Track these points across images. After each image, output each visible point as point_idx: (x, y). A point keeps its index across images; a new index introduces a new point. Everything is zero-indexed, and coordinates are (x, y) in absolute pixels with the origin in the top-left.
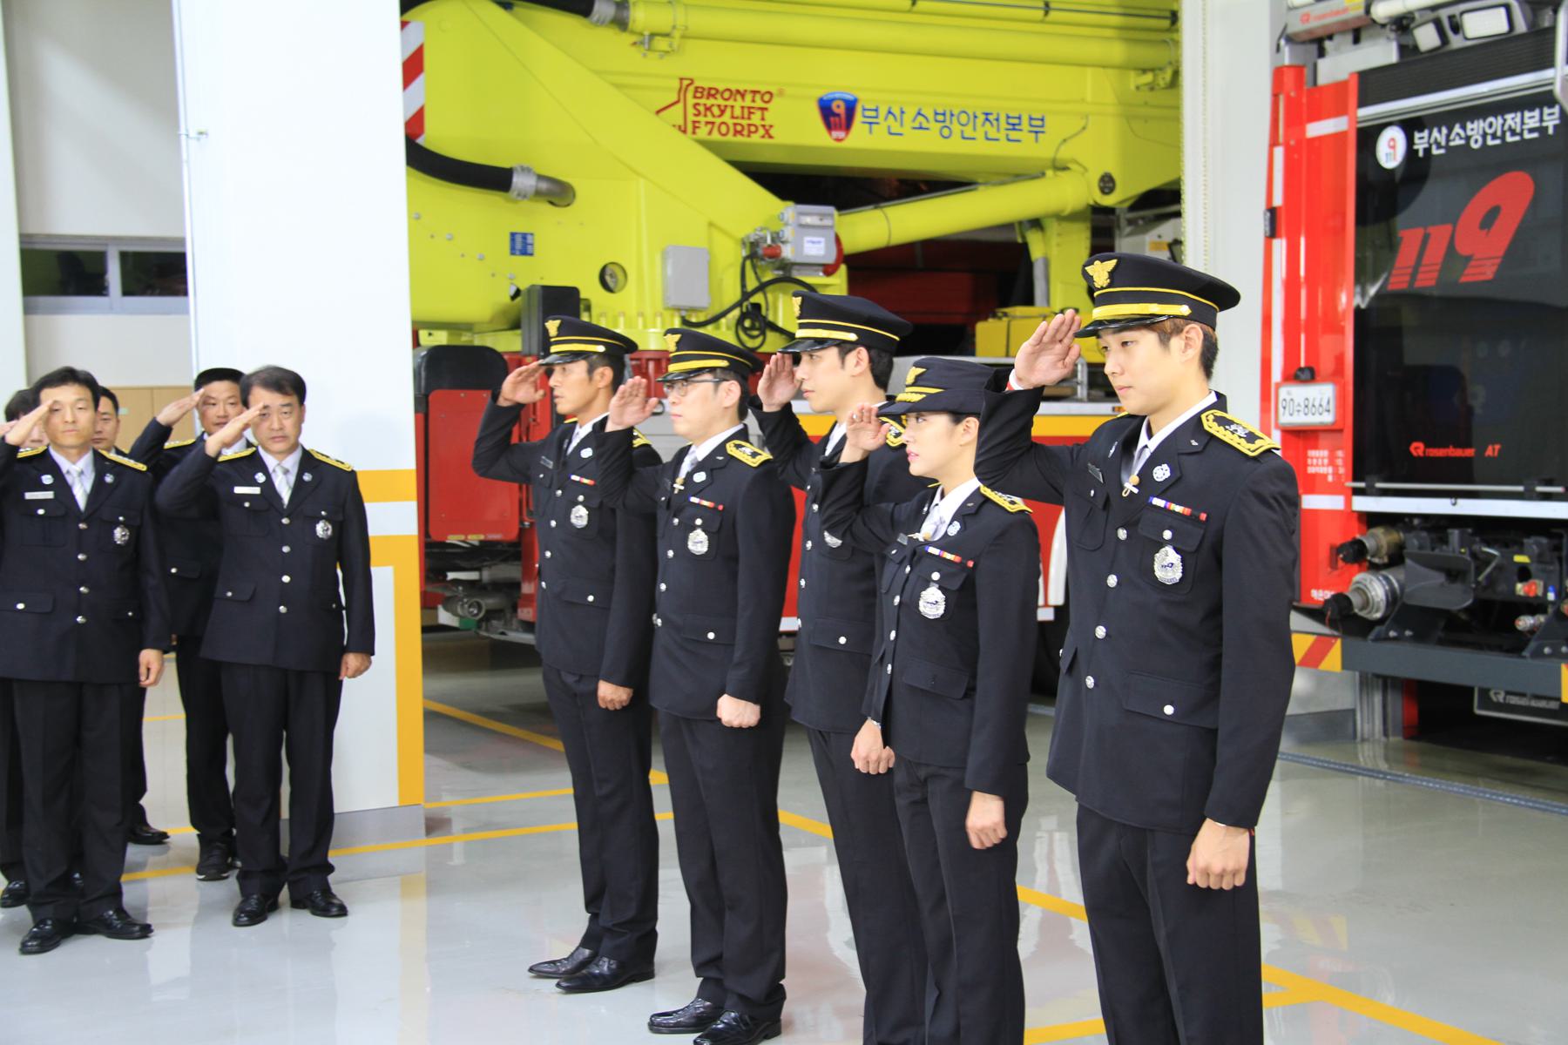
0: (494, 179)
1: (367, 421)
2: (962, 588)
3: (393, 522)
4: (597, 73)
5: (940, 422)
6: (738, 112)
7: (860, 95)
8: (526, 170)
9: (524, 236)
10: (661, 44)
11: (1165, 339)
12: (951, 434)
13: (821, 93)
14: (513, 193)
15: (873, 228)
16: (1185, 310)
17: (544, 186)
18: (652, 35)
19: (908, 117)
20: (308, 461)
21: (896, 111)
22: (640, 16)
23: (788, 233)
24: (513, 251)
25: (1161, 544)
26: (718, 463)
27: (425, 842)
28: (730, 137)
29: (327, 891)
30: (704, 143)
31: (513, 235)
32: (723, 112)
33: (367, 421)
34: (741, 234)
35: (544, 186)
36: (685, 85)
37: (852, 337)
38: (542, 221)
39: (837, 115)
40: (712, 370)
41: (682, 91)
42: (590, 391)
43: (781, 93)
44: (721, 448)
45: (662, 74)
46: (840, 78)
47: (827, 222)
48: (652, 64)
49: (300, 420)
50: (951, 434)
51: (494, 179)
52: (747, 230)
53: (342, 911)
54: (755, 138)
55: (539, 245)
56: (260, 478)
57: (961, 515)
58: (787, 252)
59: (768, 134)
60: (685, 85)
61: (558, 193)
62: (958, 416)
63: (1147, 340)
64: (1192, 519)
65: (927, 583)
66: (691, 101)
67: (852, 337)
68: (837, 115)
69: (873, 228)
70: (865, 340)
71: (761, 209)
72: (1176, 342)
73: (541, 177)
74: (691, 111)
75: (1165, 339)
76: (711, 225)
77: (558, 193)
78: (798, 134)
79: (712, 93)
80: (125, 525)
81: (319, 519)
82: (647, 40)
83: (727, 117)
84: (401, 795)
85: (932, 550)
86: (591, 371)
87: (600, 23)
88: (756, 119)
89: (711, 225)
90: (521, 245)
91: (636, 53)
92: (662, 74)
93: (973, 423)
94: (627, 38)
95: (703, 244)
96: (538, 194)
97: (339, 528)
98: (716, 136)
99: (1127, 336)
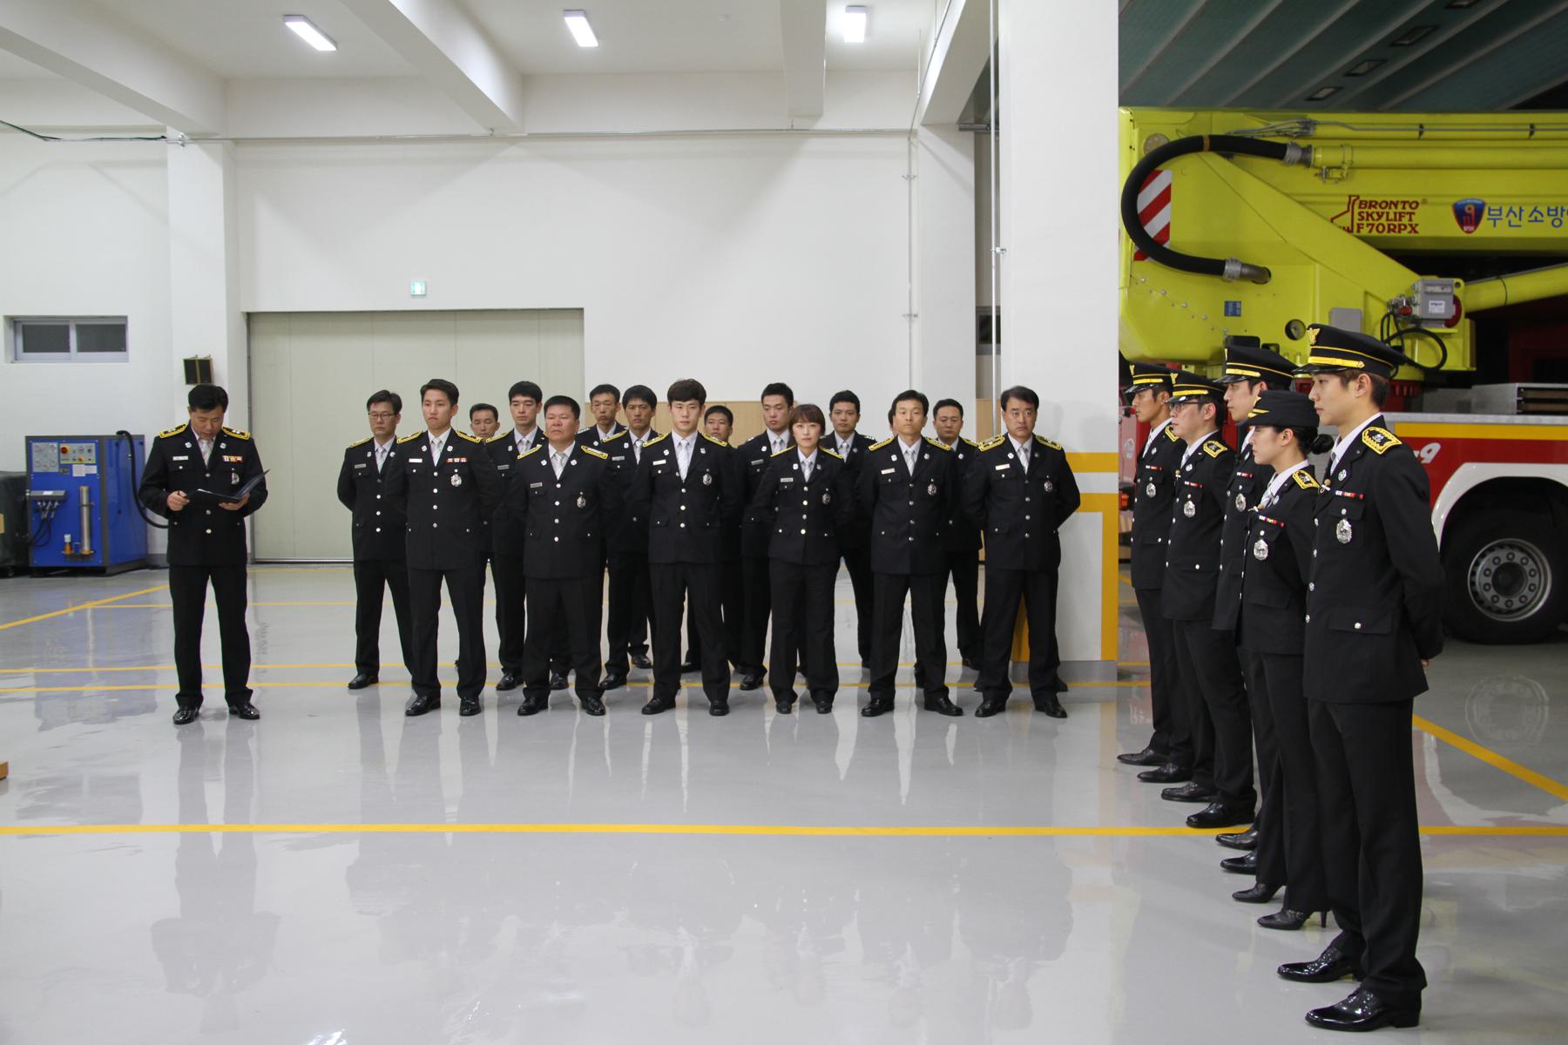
0: (1211, 267)
1: (1085, 419)
2: (1277, 540)
3: (1099, 484)
4: (1287, 195)
5: (1268, 432)
6: (1392, 216)
7: (1486, 200)
8: (1235, 261)
9: (1235, 304)
10: (1336, 174)
11: (1345, 383)
12: (1274, 440)
13: (1454, 200)
14: (1225, 276)
15: (1490, 293)
16: (1361, 364)
17: (1246, 271)
18: (1330, 168)
19: (1525, 215)
20: (1038, 446)
21: (1516, 210)
22: (1319, 157)
23: (1418, 298)
24: (1226, 314)
25: (1341, 517)
26: (1199, 458)
27: (1117, 683)
28: (1385, 234)
29: (1056, 702)
30: (1363, 239)
31: (1227, 303)
32: (1380, 217)
33: (1085, 419)
34: (1387, 299)
35: (1246, 271)
36: (1353, 201)
37: (1257, 374)
38: (1253, 298)
39: (1468, 215)
40: (1198, 396)
41: (1351, 204)
42: (1156, 408)
43: (1425, 202)
44: (1200, 448)
45: (1336, 194)
46: (1470, 188)
47: (1448, 290)
48: (1330, 187)
49: (1034, 420)
50: (1274, 440)
51: (1211, 267)
52: (1392, 296)
53: (1064, 715)
54: (1404, 234)
55: (1244, 309)
56: (1011, 456)
57: (1281, 492)
58: (1416, 311)
59: (1414, 230)
60: (1353, 201)
61: (1259, 275)
62: (1279, 428)
63: (1334, 382)
64: (1355, 499)
65: (1258, 538)
66: (1357, 210)
67: (1257, 374)
68: (1468, 215)
69: (1490, 293)
70: (1265, 377)
71: (1397, 280)
72: (1353, 385)
73: (1244, 265)
74: (1356, 216)
75: (1345, 383)
76: (1366, 293)
77: (1259, 275)
78: (1436, 226)
79: (1372, 204)
80: (1050, 480)
81: (1045, 480)
82: (1325, 173)
83: (1383, 220)
84: (1103, 654)
85: (1262, 518)
86: (1155, 395)
87: (1291, 163)
88: (1405, 220)
89: (1366, 293)
90: (1232, 309)
91: (1318, 181)
92: (1336, 194)
93: (1289, 432)
94: (1312, 171)
95: (1361, 307)
96: (1242, 277)
97: (1056, 485)
98: (1375, 233)
99: (1323, 377)
